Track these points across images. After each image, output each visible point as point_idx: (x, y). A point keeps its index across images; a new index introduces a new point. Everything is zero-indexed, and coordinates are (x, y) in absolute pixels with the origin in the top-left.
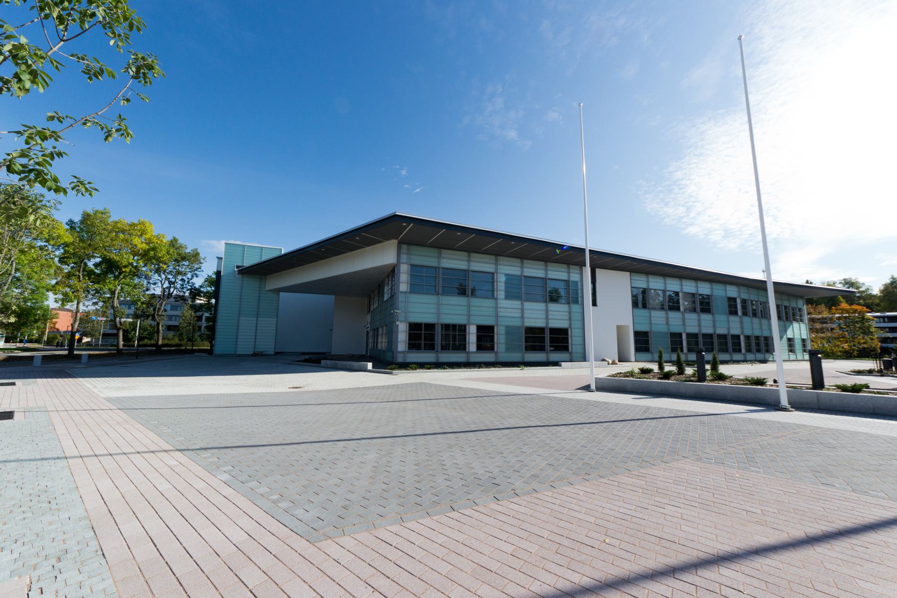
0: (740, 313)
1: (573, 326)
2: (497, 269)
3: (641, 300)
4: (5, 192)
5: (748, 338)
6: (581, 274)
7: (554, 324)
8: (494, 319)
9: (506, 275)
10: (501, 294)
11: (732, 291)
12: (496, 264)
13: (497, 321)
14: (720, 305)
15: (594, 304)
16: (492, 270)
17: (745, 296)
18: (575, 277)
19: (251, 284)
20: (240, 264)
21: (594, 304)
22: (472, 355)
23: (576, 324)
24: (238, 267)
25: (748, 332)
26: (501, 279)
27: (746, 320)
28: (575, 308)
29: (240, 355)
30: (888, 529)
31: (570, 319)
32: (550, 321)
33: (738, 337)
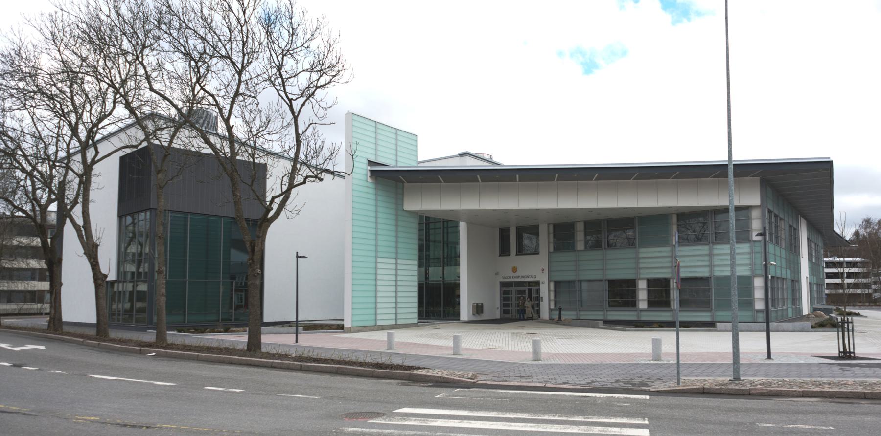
20: (373, 159)
24: (370, 163)
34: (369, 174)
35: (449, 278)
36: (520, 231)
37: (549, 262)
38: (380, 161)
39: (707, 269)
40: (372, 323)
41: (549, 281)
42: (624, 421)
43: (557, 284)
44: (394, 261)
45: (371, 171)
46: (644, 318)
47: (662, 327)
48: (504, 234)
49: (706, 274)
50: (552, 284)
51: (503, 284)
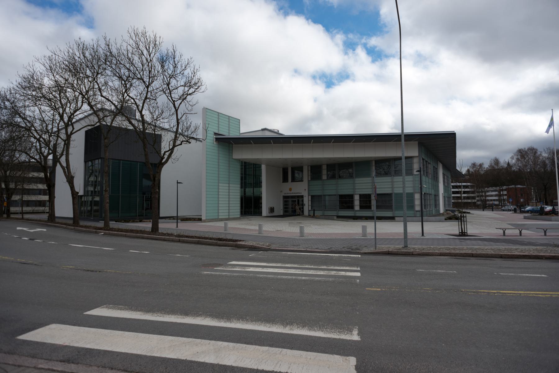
20: (217, 132)
24: (215, 134)
36: (293, 169)
37: (309, 185)
40: (217, 217)
41: (309, 195)
43: (313, 197)
44: (228, 185)
48: (285, 171)
50: (310, 197)
51: (285, 197)
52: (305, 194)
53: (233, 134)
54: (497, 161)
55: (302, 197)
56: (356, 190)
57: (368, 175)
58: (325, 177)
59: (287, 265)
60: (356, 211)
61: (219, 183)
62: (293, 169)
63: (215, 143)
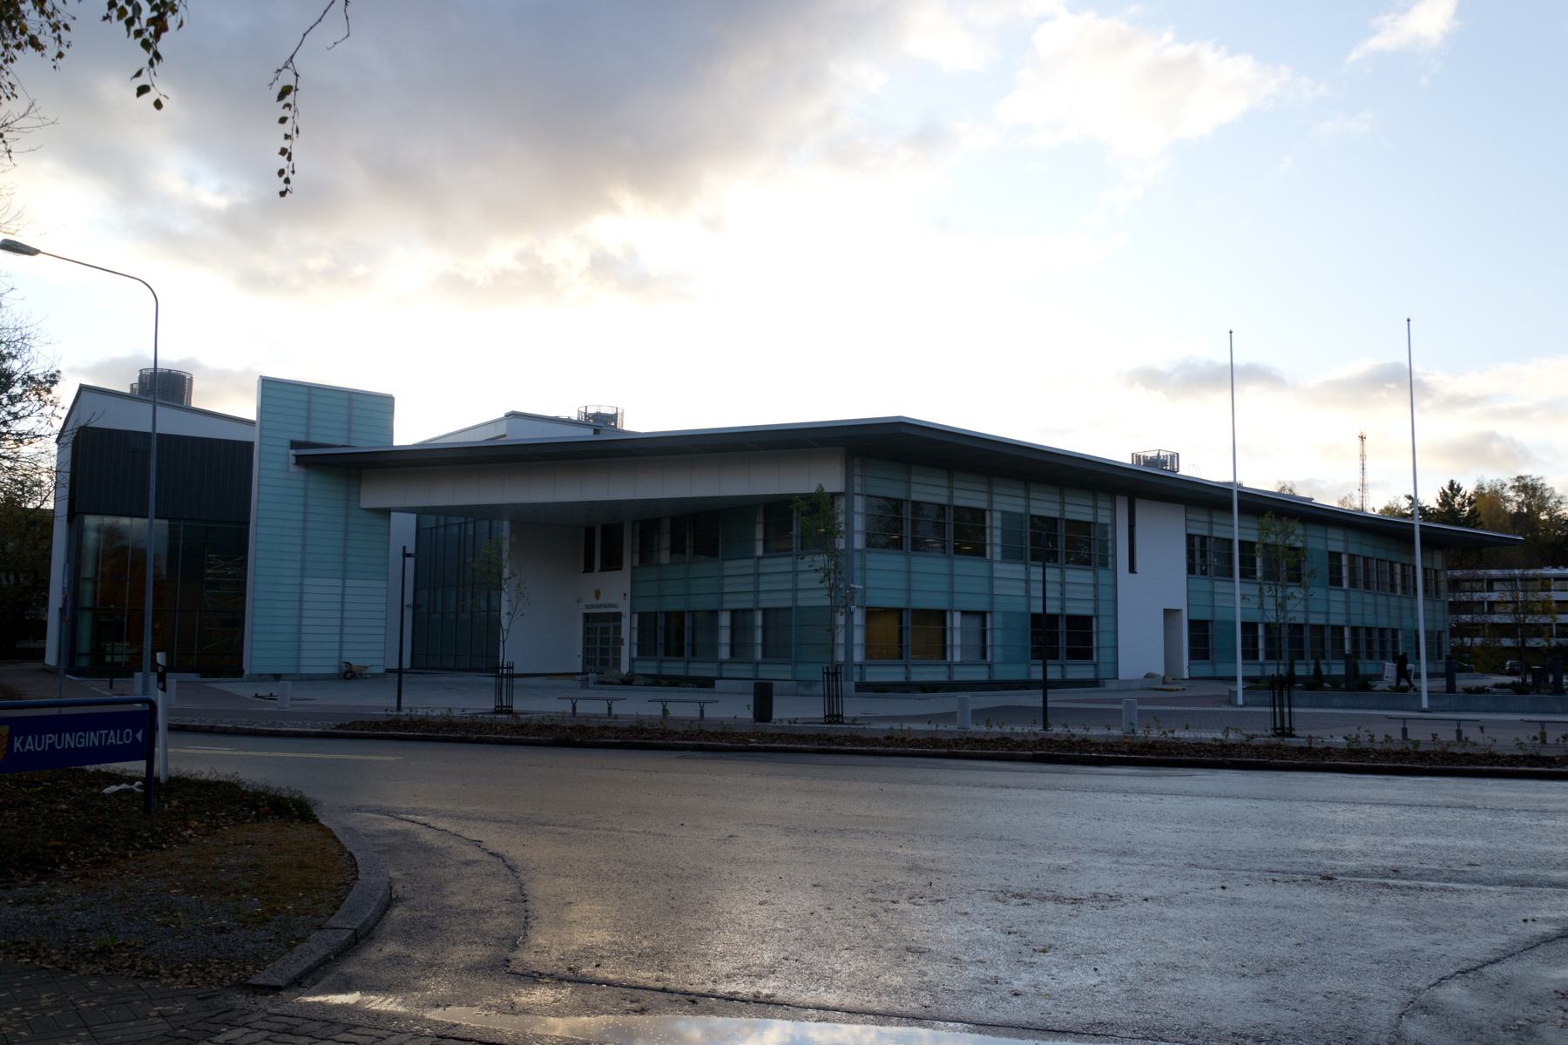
0: (1345, 585)
1: (1101, 612)
2: (990, 501)
3: (1204, 558)
4: (1558, 689)
5: (1355, 630)
6: (1114, 510)
7: (1074, 609)
8: (1091, 605)
9: (1003, 513)
10: (995, 548)
11: (1336, 541)
12: (990, 493)
13: (992, 603)
14: (1317, 565)
15: (1132, 569)
16: (982, 505)
17: (1354, 549)
18: (1104, 517)
19: (325, 495)
20: (301, 438)
21: (1132, 569)
22: (956, 669)
23: (1105, 609)
24: (295, 445)
25: (1356, 621)
26: (995, 522)
27: (1355, 596)
28: (1104, 576)
29: (311, 678)
30: (1302, 492)
31: (1096, 600)
32: (1068, 604)
33: (1341, 628)
34: (293, 460)
35: (1202, 584)
36: (605, 528)
37: (633, 582)
38: (314, 439)
39: (788, 595)
40: (293, 670)
41: (632, 613)
42: (66, 711)
43: (642, 616)
44: (339, 582)
45: (297, 457)
46: (957, 678)
47: (676, 685)
48: (590, 532)
49: (789, 604)
50: (636, 617)
51: (587, 617)
52: (624, 607)
53: (364, 443)
54: (1481, 487)
55: (617, 617)
56: (726, 598)
57: (748, 554)
58: (759, 551)
59: (54, 711)
60: (722, 663)
61: (302, 577)
62: (605, 528)
63: (293, 469)
